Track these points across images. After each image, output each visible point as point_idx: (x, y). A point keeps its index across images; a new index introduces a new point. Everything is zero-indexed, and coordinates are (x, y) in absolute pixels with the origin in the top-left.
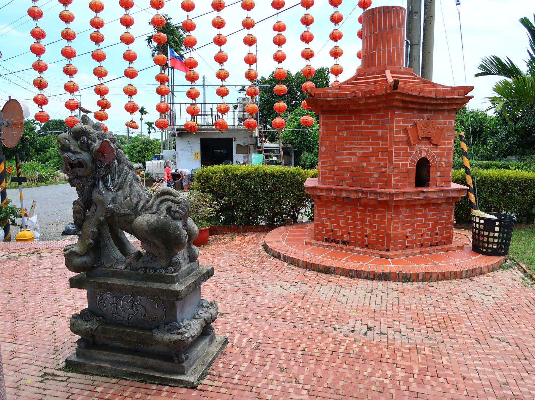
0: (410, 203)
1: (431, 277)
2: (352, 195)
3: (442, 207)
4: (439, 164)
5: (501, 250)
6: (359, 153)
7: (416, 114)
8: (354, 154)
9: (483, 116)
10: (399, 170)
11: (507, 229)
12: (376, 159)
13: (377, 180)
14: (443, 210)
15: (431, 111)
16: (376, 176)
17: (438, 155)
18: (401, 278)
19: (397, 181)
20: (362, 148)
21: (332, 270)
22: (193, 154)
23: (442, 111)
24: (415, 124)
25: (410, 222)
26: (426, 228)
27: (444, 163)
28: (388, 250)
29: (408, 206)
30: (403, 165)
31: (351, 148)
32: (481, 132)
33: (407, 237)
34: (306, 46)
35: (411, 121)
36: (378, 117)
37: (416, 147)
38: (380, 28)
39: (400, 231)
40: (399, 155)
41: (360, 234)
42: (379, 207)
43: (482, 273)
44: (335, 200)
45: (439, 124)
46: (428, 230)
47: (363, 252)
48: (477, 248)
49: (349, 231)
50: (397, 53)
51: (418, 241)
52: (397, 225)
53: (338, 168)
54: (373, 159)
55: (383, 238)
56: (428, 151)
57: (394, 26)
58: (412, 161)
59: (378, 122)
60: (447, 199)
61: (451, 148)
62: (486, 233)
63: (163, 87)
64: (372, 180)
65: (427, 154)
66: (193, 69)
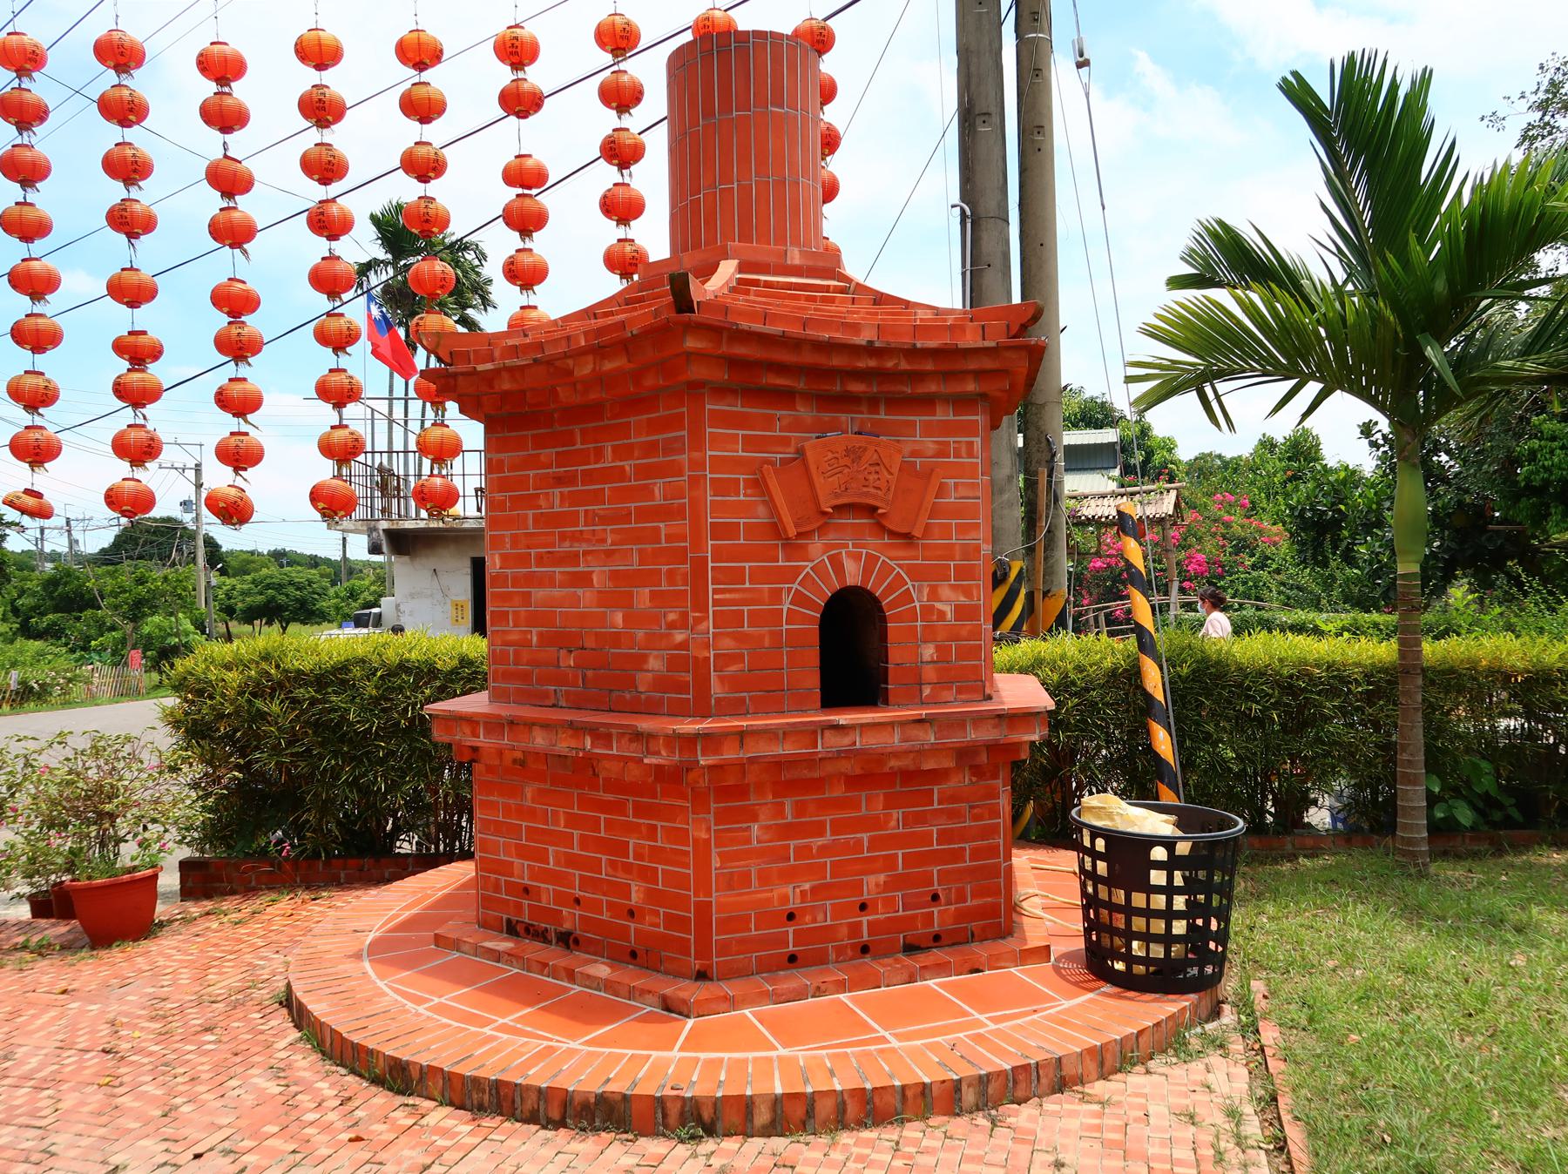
0: (785, 776)
1: (810, 1113)
2: (564, 745)
3: (952, 784)
4: (928, 611)
5: (1189, 971)
6: (599, 574)
7: (805, 412)
8: (584, 580)
9: (1342, 474)
10: (741, 638)
11: (1210, 873)
12: (653, 595)
13: (661, 683)
14: (954, 798)
15: (873, 403)
16: (655, 663)
17: (916, 574)
18: (673, 1118)
19: (734, 683)
20: (609, 554)
21: (415, 1074)
22: (449, 607)
23: (927, 403)
24: (801, 452)
25: (802, 852)
26: (882, 878)
27: (948, 609)
28: (702, 976)
29: (786, 788)
30: (755, 618)
31: (576, 554)
32: (1335, 525)
33: (791, 916)
34: (621, 232)
35: (785, 442)
36: (653, 426)
37: (816, 546)
38: (709, 113)
39: (756, 892)
40: (737, 576)
41: (610, 905)
42: (665, 794)
43: (1062, 1085)
44: (522, 763)
45: (915, 454)
46: (894, 884)
47: (608, 985)
48: (1101, 962)
49: (578, 893)
51: (845, 930)
52: (736, 867)
53: (540, 635)
54: (642, 597)
55: (682, 923)
56: (872, 560)
58: (799, 599)
59: (651, 449)
60: (965, 754)
61: (978, 548)
62: (1120, 896)
63: (136, 376)
64: (643, 680)
65: (867, 572)
66: (243, 319)
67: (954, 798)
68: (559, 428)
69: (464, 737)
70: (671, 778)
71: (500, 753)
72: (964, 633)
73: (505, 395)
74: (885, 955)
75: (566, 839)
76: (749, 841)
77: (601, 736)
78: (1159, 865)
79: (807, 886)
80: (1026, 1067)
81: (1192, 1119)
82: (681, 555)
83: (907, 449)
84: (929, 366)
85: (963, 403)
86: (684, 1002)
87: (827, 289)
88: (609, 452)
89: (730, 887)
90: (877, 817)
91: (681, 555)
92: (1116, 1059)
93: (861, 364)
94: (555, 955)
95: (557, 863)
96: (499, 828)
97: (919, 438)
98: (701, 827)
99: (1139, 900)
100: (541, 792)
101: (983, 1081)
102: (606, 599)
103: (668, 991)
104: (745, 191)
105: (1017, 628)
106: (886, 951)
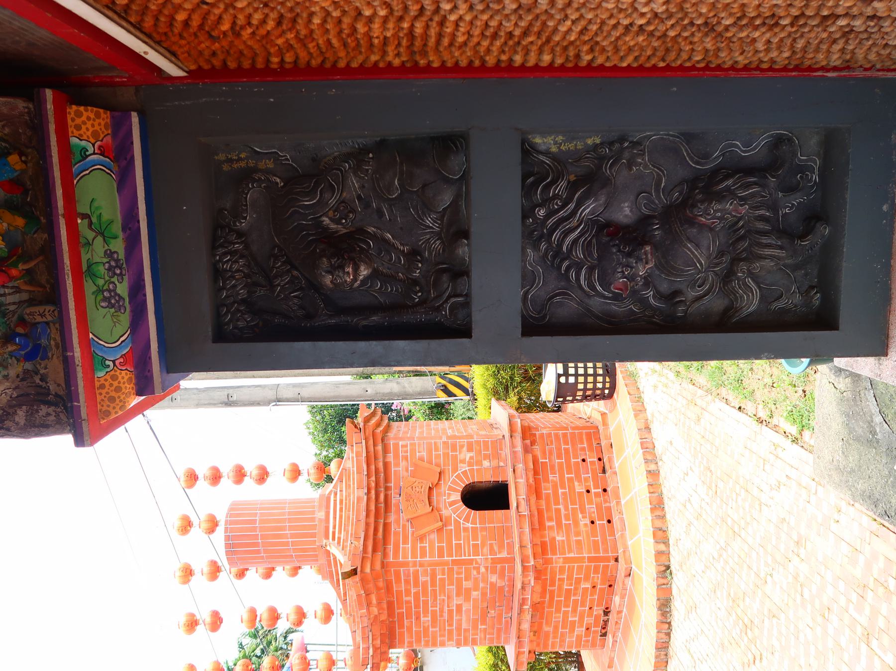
0: (537, 526)
2: (527, 617)
3: (539, 454)
4: (470, 464)
7: (392, 518)
8: (459, 607)
13: (502, 576)
15: (387, 489)
16: (494, 578)
17: (455, 469)
18: (665, 581)
20: (449, 597)
23: (386, 465)
25: (567, 519)
26: (576, 483)
27: (469, 455)
28: (617, 560)
30: (475, 538)
33: (593, 522)
35: (404, 526)
37: (445, 513)
38: (258, 552)
42: (546, 575)
43: (648, 428)
44: (535, 632)
45: (407, 470)
47: (623, 597)
48: (608, 394)
49: (587, 608)
50: (297, 520)
51: (598, 500)
52: (574, 546)
53: (482, 624)
54: (466, 584)
56: (450, 489)
57: (254, 529)
58: (467, 520)
59: (407, 582)
60: (526, 450)
64: (500, 583)
65: (455, 490)
67: (544, 453)
68: (396, 619)
69: (525, 658)
70: (539, 574)
71: (531, 641)
72: (478, 448)
73: (382, 642)
74: (606, 482)
75: (566, 613)
76: (563, 541)
77: (523, 602)
78: (567, 379)
79: (580, 516)
80: (642, 444)
81: (655, 387)
82: (451, 570)
83: (405, 474)
84: (373, 467)
85: (386, 450)
86: (626, 569)
87: (335, 501)
88: (408, 598)
89: (582, 549)
90: (553, 486)
91: (451, 570)
92: (639, 409)
93: (374, 497)
94: (612, 617)
95: (575, 616)
96: (562, 641)
97: (400, 470)
98: (557, 560)
99: (581, 386)
100: (547, 623)
101: (647, 461)
102: (467, 598)
103: (623, 575)
104: (292, 536)
105: (467, 380)
106: (605, 480)
